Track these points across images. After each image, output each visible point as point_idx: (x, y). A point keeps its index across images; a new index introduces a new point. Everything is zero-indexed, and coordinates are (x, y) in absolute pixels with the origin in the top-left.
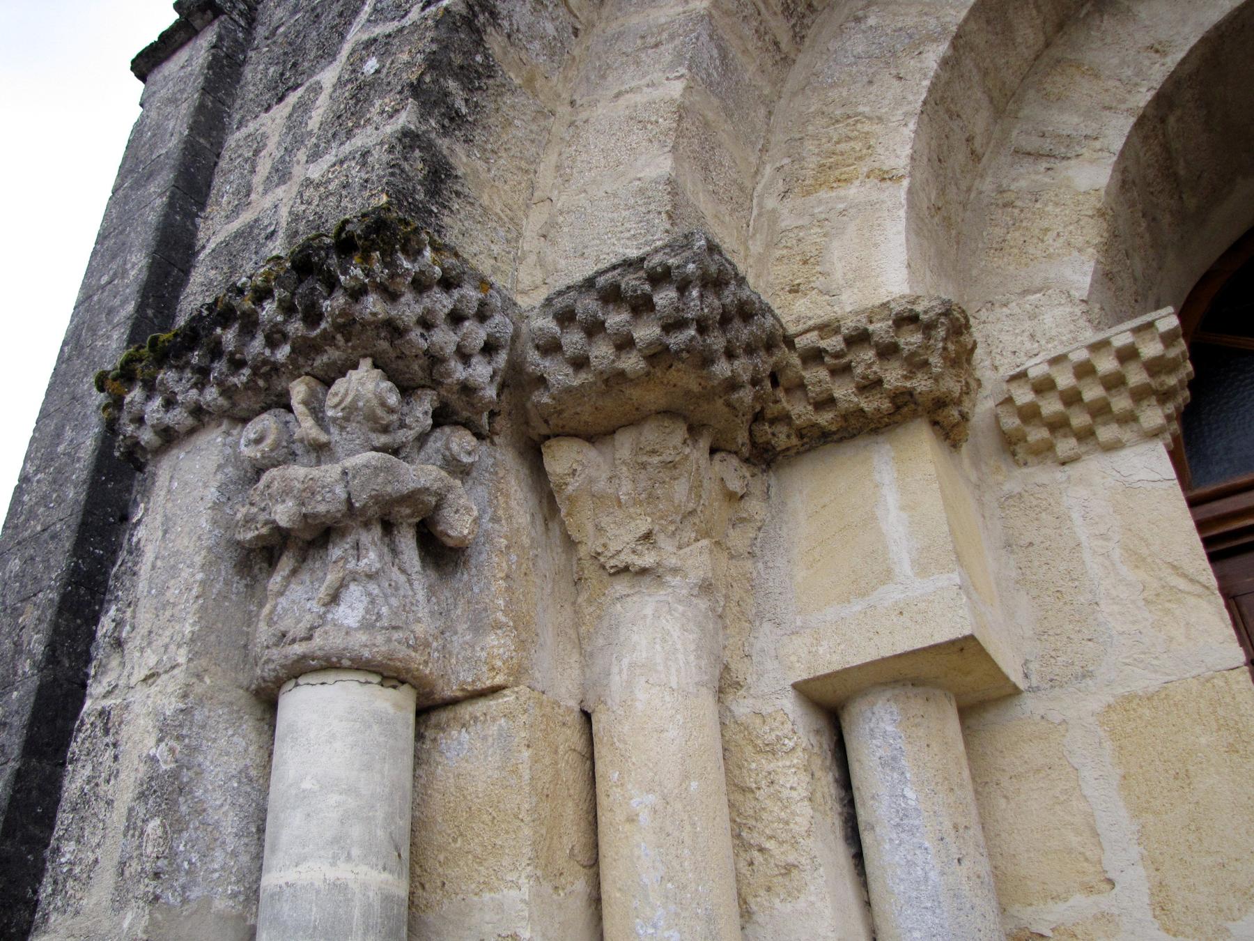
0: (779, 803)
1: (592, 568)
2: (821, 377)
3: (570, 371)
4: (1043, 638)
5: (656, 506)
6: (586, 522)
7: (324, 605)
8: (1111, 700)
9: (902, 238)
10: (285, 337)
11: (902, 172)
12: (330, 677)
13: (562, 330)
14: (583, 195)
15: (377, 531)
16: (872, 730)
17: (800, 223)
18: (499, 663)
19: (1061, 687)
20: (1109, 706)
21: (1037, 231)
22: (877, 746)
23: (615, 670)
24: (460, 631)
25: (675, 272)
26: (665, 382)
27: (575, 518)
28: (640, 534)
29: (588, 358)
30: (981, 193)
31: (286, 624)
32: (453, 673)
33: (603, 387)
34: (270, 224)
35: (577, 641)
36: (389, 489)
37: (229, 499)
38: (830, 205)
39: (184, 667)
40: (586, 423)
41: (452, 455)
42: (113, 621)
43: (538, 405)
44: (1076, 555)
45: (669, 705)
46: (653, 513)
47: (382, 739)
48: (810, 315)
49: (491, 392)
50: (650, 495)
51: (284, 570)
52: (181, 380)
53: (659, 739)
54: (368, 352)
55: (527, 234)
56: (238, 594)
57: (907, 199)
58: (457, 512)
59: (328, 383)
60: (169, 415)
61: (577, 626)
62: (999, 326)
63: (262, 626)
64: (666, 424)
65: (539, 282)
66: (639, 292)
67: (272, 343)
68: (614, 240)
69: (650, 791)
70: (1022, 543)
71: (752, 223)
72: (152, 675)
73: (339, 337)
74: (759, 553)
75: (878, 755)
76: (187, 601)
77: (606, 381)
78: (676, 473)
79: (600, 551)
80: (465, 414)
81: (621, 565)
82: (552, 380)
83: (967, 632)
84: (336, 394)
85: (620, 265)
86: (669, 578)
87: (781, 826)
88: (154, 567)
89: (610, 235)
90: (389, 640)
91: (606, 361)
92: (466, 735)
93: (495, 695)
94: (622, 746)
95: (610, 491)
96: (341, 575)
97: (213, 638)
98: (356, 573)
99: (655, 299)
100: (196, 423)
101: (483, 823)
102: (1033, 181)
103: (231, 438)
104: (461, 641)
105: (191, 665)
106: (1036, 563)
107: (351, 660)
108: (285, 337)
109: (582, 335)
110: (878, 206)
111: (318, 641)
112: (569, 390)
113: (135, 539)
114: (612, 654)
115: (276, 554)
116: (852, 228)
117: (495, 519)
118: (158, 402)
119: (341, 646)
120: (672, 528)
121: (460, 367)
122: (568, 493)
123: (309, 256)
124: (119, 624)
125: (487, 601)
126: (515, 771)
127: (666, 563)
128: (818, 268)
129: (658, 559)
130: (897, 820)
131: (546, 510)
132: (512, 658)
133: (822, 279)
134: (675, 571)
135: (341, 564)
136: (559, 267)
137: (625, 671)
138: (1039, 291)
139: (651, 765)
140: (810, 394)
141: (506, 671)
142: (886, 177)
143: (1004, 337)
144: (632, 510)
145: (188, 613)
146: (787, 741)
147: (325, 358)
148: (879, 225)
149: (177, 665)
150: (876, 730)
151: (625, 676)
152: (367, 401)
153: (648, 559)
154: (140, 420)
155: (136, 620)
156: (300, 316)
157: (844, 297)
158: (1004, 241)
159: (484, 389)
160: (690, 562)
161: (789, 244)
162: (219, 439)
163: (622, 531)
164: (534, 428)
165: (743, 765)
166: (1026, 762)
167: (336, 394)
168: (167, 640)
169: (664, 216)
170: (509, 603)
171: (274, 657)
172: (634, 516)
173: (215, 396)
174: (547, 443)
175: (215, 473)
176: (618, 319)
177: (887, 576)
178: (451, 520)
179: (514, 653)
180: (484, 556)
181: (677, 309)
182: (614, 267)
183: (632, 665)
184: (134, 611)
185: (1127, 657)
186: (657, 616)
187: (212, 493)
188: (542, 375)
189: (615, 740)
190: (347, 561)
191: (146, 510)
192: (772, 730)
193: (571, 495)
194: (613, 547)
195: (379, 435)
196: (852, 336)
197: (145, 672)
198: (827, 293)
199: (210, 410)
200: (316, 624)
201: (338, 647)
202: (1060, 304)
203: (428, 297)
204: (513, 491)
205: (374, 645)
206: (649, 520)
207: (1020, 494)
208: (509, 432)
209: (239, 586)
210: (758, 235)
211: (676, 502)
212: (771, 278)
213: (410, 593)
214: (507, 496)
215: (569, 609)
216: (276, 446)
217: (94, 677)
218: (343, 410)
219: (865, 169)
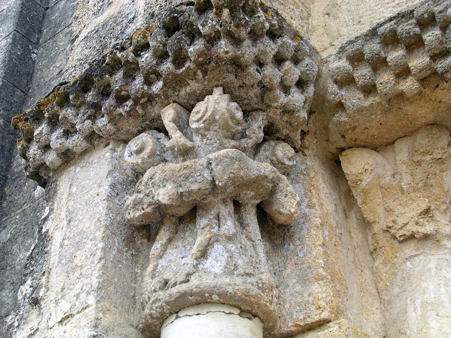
1: (385, 239)
3: (362, 96)
5: (431, 191)
6: (377, 207)
7: (196, 259)
10: (158, 76)
12: (203, 310)
13: (353, 68)
15: (231, 207)
18: (323, 304)
24: (291, 284)
25: (438, 17)
26: (433, 98)
27: (368, 205)
29: (375, 86)
31: (168, 275)
32: (287, 314)
33: (387, 105)
34: (131, 13)
35: (376, 294)
36: (242, 173)
37: (117, 194)
39: (94, 306)
40: (373, 136)
41: (277, 159)
42: (30, 287)
43: (339, 123)
46: (428, 197)
49: (304, 115)
50: (425, 185)
51: (162, 240)
54: (220, 83)
55: (314, 13)
56: (126, 260)
58: (286, 196)
59: (189, 109)
60: (68, 141)
61: (376, 283)
63: (147, 279)
64: (434, 132)
65: (327, 45)
66: (412, 34)
67: (148, 82)
72: (67, 317)
73: (199, 72)
76: (93, 262)
77: (389, 101)
78: (444, 167)
79: (390, 225)
80: (285, 132)
81: (408, 234)
82: (348, 104)
84: (198, 112)
85: (395, 17)
88: (61, 246)
89: (379, 7)
90: (245, 283)
91: (389, 86)
93: (322, 327)
96: (208, 236)
97: (112, 288)
98: (219, 235)
99: (424, 37)
100: (89, 145)
105: (99, 305)
107: (219, 295)
108: (158, 76)
109: (369, 69)
111: (194, 281)
112: (360, 110)
113: (44, 230)
114: (407, 298)
115: (153, 232)
117: (310, 206)
118: (60, 131)
119: (212, 285)
120: (444, 207)
121: (283, 95)
123: (176, 18)
124: (35, 288)
125: (310, 261)
127: (442, 231)
129: (436, 228)
131: (344, 204)
132: (332, 301)
135: (208, 229)
136: (342, 33)
137: (419, 308)
141: (329, 310)
144: (413, 195)
145: (95, 270)
147: (188, 89)
149: (88, 306)
151: (419, 312)
152: (222, 115)
153: (429, 228)
154: (47, 148)
155: (50, 283)
156: (170, 59)
159: (299, 111)
162: (108, 154)
163: (407, 210)
164: (333, 144)
167: (198, 112)
168: (78, 291)
170: (326, 263)
171: (160, 298)
173: (105, 123)
174: (344, 153)
175: (107, 176)
176: (396, 54)
178: (283, 201)
179: (333, 298)
180: (305, 231)
181: (441, 43)
182: (391, 19)
183: (424, 304)
184: (48, 277)
186: (439, 268)
187: (105, 189)
188: (340, 101)
191: (51, 210)
193: (365, 189)
194: (400, 222)
195: (230, 140)
197: (61, 316)
199: (101, 134)
200: (191, 272)
201: (209, 286)
203: (262, 42)
204: (321, 187)
205: (235, 284)
206: (427, 200)
208: (314, 147)
209: (128, 255)
213: (254, 254)
214: (318, 190)
215: (367, 273)
216: (152, 154)
217: (18, 327)
218: (204, 122)
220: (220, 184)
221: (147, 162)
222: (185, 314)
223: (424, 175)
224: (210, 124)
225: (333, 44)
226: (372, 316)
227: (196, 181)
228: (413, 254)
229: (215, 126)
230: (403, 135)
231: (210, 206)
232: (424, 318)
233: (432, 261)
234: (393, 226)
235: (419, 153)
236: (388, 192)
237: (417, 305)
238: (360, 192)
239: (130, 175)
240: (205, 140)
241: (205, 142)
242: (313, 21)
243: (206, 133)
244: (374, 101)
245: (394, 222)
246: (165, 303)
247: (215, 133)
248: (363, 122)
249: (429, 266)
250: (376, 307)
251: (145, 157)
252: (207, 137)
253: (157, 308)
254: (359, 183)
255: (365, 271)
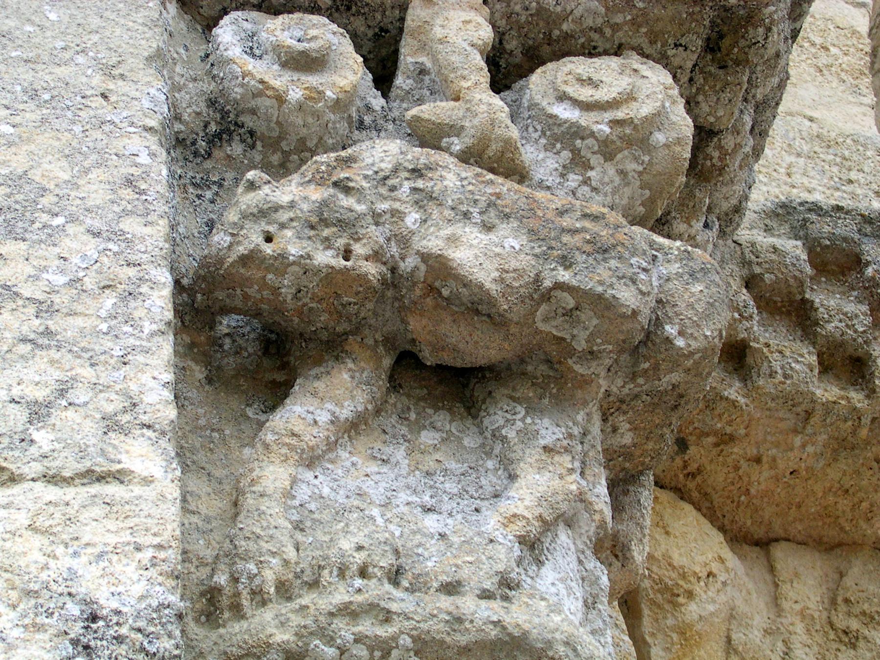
193: (690, 626)
218: (615, 123)
220: (680, 343)
221: (317, 115)
224: (629, 142)
227: (634, 282)
229: (636, 159)
230: (799, 538)
231: (579, 394)
235: (856, 610)
238: (673, 629)
239: (186, 117)
240: (574, 179)
241: (573, 184)
243: (595, 160)
244: (842, 398)
246: (415, 639)
247: (617, 180)
248: (760, 437)
251: (329, 93)
252: (590, 174)
253: (356, 641)
254: (681, 600)
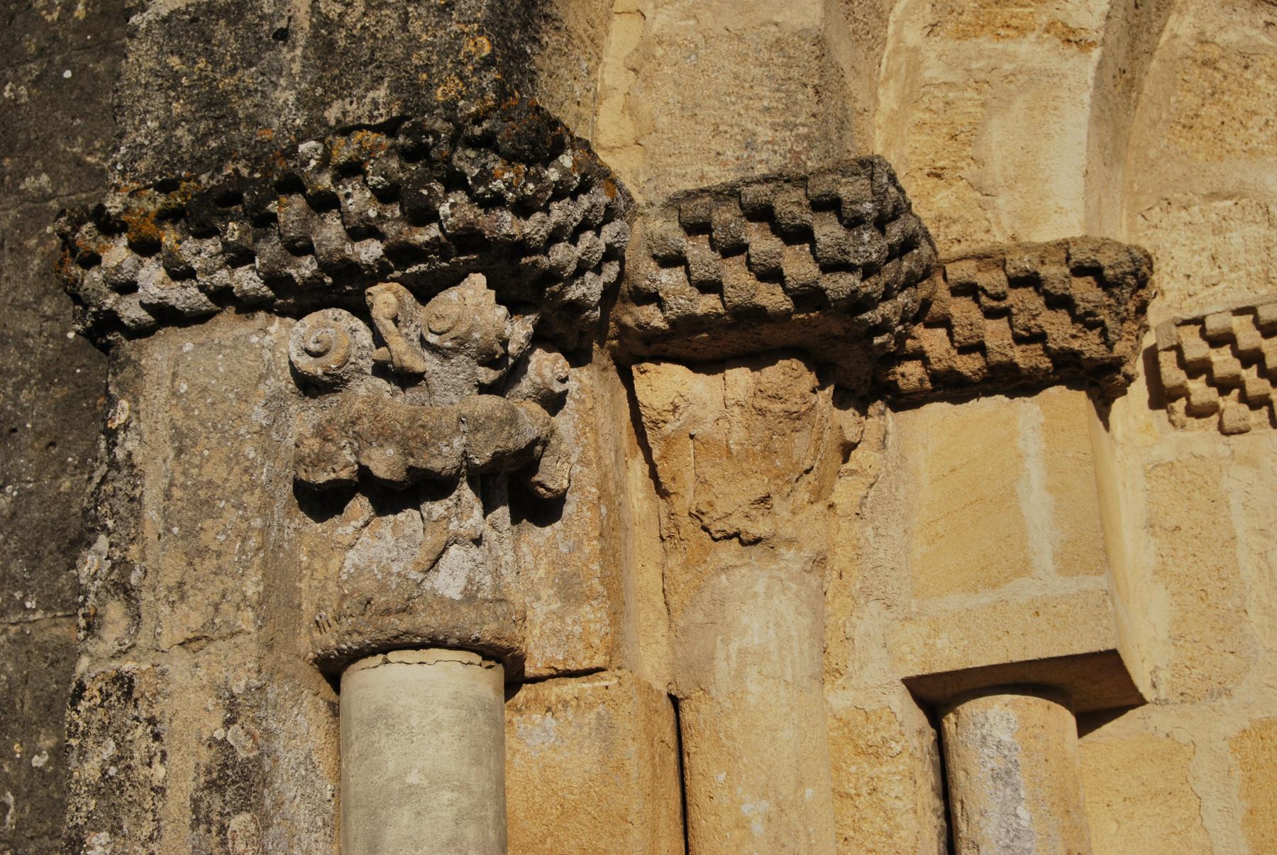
0: (882, 814)
2: (974, 320)
4: (1178, 643)
5: (773, 462)
8: (1248, 725)
9: (1083, 133)
11: (1093, 37)
14: (692, 22)
16: (984, 737)
17: (951, 78)
18: (596, 641)
19: (1193, 703)
20: (1245, 731)
21: (1241, 112)
22: (988, 756)
23: (720, 654)
24: (544, 597)
28: (759, 496)
30: (1176, 36)
35: (665, 611)
36: (511, 445)
38: (993, 61)
44: (1228, 550)
45: (784, 701)
47: (487, 729)
48: (955, 216)
52: (199, 252)
53: (773, 740)
57: (1096, 79)
62: (1173, 235)
64: (794, 366)
68: (739, 107)
69: (765, 796)
70: (1167, 525)
71: (884, 61)
74: (868, 515)
75: (989, 766)
81: (731, 532)
83: (1110, 647)
86: (782, 550)
87: (883, 839)
92: (554, 722)
93: (590, 677)
94: (729, 743)
95: (718, 437)
101: (580, 823)
102: (1247, 36)
103: (268, 338)
104: (546, 609)
106: (1181, 553)
110: (1056, 79)
114: (716, 635)
116: (1019, 104)
120: (787, 489)
122: (666, 433)
126: (620, 767)
128: (969, 151)
130: (1007, 841)
133: (974, 167)
134: (790, 542)
136: (659, 125)
137: (734, 657)
138: (1229, 197)
139: (765, 768)
140: (956, 338)
142: (1072, 38)
143: (1177, 252)
146: (893, 744)
148: (1055, 109)
150: (989, 738)
153: (760, 527)
157: (1000, 201)
158: (1197, 116)
160: (805, 532)
161: (933, 107)
165: (841, 767)
166: (1143, 784)
169: (810, 90)
172: (749, 473)
177: (1024, 567)
182: (766, 180)
183: (742, 652)
185: (1270, 678)
186: (769, 595)
189: (721, 735)
190: (450, 521)
192: (876, 729)
193: (668, 436)
194: (722, 507)
196: (1018, 277)
198: (980, 190)
202: (1254, 222)
207: (1172, 464)
210: (891, 82)
211: (795, 458)
212: (907, 151)
219: (1045, 19)
222: (399, 660)
223: (767, 432)
225: (641, 142)
226: (654, 646)
227: (440, 455)
228: (731, 563)
232: (739, 675)
233: (761, 580)
234: (708, 513)
235: (765, 395)
236: (706, 449)
237: (731, 651)
238: (661, 439)
242: (605, 76)
245: (711, 504)
249: (755, 589)
250: (661, 633)
255: (648, 566)
